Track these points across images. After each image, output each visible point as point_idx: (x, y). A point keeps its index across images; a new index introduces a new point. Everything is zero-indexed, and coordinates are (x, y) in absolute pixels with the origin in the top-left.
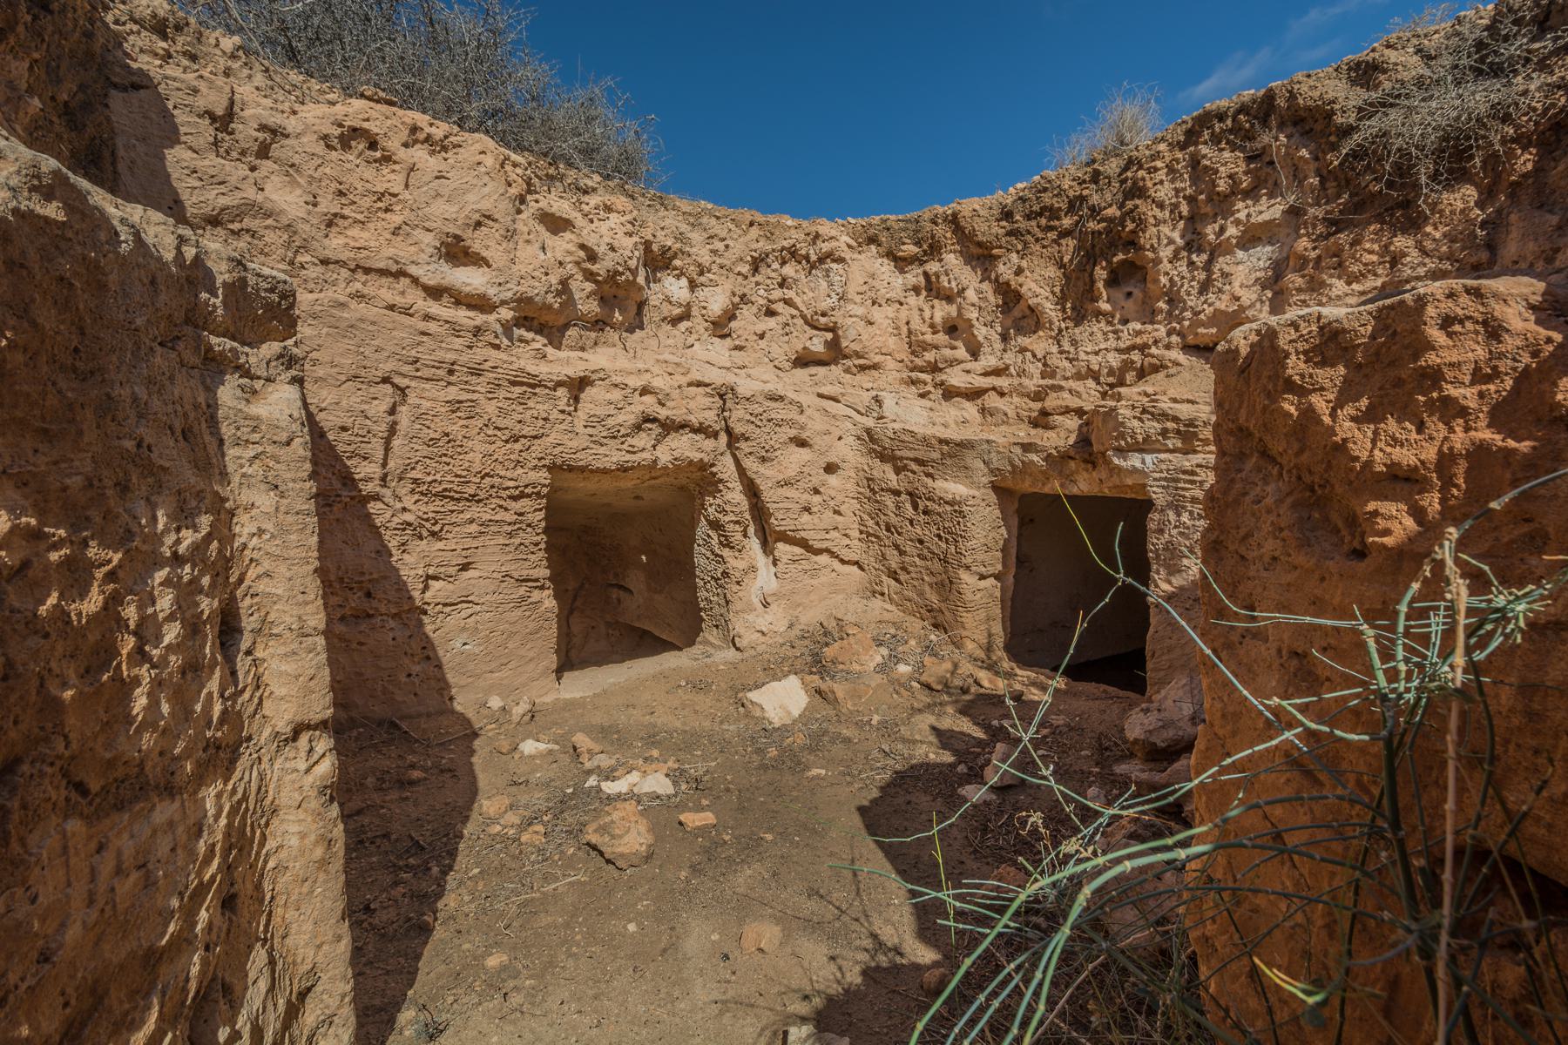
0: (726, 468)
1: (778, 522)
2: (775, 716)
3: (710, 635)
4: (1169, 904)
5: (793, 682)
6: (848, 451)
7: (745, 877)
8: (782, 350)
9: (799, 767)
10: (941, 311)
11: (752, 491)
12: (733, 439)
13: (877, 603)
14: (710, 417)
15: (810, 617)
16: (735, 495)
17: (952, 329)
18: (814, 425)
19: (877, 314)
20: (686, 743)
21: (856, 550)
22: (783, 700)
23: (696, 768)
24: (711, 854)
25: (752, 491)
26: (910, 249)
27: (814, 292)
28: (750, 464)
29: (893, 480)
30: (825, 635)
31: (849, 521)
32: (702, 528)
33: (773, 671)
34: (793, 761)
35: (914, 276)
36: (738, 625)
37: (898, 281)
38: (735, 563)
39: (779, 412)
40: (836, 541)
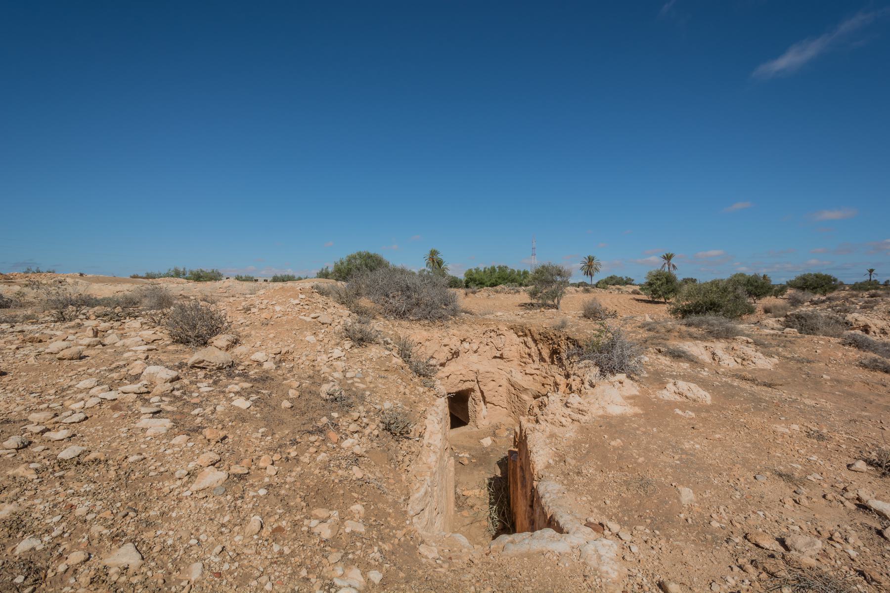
0: (476, 388)
1: (487, 400)
2: (485, 445)
3: (471, 423)
4: (171, 348)
5: (489, 438)
6: (505, 383)
7: (480, 468)
8: (490, 355)
9: (489, 454)
10: (527, 350)
11: (482, 392)
12: (478, 382)
13: (510, 418)
14: (474, 378)
15: (495, 421)
16: (479, 394)
17: (529, 355)
18: (496, 377)
19: (513, 348)
20: (470, 449)
21: (505, 405)
22: (487, 442)
23: (473, 453)
24: (476, 465)
25: (482, 392)
26: (521, 334)
27: (498, 342)
28: (482, 387)
29: (514, 391)
30: (497, 427)
31: (504, 398)
32: (470, 399)
33: (485, 435)
34: (488, 453)
35: (521, 339)
36: (478, 423)
37: (518, 339)
38: (478, 409)
39: (488, 375)
40: (501, 403)
